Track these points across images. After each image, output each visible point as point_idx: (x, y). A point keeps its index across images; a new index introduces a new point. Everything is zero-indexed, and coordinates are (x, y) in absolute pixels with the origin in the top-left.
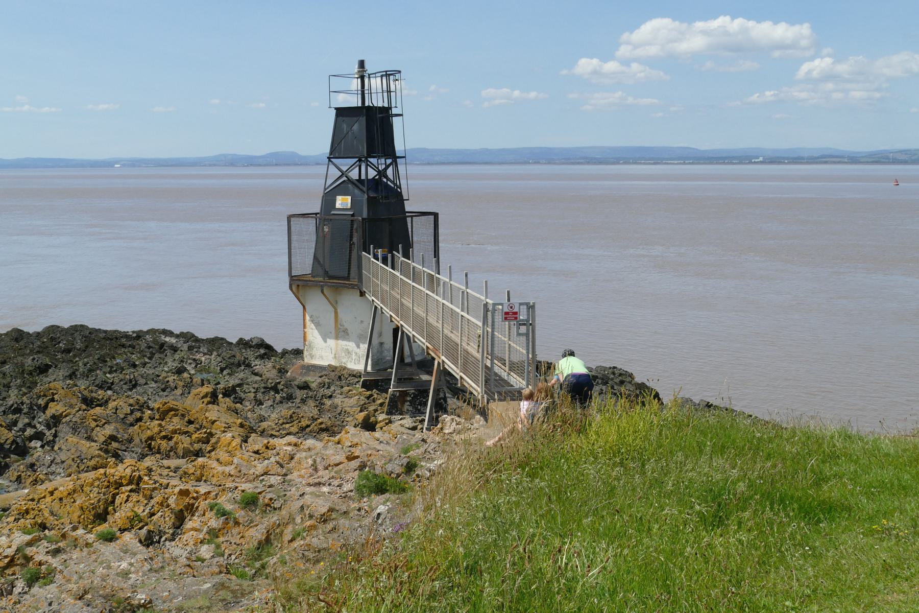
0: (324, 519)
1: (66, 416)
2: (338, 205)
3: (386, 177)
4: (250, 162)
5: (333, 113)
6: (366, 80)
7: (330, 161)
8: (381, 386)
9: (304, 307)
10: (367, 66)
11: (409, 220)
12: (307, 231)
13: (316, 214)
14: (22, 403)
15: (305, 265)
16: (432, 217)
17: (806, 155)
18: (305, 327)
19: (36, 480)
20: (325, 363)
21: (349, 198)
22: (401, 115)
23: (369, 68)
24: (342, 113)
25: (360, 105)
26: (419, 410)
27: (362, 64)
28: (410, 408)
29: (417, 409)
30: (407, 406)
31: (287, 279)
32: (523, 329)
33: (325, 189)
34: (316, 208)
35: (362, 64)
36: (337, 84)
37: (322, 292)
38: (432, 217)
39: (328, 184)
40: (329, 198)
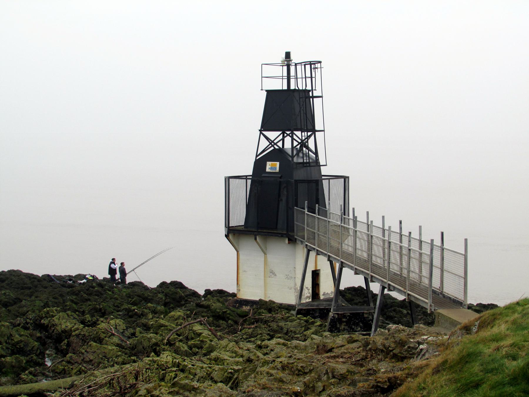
1: (75, 331)
2: (268, 170)
3: (307, 148)
5: (263, 95)
6: (292, 68)
7: (261, 133)
8: (312, 314)
9: (237, 252)
10: (292, 57)
11: (325, 183)
12: (241, 193)
13: (246, 177)
14: (27, 323)
15: (239, 218)
16: (230, 180)
19: (79, 371)
21: (278, 164)
22: (321, 97)
23: (295, 59)
24: (270, 94)
25: (285, 88)
26: (353, 329)
28: (346, 328)
29: (351, 328)
31: (223, 231)
33: (257, 156)
34: (249, 171)
36: (269, 71)
37: (256, 239)
38: (230, 180)
39: (258, 154)
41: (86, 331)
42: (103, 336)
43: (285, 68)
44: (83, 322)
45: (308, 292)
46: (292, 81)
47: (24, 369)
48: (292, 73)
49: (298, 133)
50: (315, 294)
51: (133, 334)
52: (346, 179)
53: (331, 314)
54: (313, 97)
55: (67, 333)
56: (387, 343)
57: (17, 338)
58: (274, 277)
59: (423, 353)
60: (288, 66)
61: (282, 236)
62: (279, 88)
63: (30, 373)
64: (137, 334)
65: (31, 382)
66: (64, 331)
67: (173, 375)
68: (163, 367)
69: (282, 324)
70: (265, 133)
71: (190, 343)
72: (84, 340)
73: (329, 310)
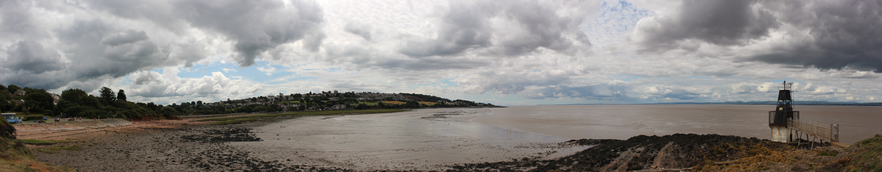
4: (732, 103)
12: (773, 115)
15: (772, 122)
40: (778, 108)
55: (732, 149)
58: (780, 135)
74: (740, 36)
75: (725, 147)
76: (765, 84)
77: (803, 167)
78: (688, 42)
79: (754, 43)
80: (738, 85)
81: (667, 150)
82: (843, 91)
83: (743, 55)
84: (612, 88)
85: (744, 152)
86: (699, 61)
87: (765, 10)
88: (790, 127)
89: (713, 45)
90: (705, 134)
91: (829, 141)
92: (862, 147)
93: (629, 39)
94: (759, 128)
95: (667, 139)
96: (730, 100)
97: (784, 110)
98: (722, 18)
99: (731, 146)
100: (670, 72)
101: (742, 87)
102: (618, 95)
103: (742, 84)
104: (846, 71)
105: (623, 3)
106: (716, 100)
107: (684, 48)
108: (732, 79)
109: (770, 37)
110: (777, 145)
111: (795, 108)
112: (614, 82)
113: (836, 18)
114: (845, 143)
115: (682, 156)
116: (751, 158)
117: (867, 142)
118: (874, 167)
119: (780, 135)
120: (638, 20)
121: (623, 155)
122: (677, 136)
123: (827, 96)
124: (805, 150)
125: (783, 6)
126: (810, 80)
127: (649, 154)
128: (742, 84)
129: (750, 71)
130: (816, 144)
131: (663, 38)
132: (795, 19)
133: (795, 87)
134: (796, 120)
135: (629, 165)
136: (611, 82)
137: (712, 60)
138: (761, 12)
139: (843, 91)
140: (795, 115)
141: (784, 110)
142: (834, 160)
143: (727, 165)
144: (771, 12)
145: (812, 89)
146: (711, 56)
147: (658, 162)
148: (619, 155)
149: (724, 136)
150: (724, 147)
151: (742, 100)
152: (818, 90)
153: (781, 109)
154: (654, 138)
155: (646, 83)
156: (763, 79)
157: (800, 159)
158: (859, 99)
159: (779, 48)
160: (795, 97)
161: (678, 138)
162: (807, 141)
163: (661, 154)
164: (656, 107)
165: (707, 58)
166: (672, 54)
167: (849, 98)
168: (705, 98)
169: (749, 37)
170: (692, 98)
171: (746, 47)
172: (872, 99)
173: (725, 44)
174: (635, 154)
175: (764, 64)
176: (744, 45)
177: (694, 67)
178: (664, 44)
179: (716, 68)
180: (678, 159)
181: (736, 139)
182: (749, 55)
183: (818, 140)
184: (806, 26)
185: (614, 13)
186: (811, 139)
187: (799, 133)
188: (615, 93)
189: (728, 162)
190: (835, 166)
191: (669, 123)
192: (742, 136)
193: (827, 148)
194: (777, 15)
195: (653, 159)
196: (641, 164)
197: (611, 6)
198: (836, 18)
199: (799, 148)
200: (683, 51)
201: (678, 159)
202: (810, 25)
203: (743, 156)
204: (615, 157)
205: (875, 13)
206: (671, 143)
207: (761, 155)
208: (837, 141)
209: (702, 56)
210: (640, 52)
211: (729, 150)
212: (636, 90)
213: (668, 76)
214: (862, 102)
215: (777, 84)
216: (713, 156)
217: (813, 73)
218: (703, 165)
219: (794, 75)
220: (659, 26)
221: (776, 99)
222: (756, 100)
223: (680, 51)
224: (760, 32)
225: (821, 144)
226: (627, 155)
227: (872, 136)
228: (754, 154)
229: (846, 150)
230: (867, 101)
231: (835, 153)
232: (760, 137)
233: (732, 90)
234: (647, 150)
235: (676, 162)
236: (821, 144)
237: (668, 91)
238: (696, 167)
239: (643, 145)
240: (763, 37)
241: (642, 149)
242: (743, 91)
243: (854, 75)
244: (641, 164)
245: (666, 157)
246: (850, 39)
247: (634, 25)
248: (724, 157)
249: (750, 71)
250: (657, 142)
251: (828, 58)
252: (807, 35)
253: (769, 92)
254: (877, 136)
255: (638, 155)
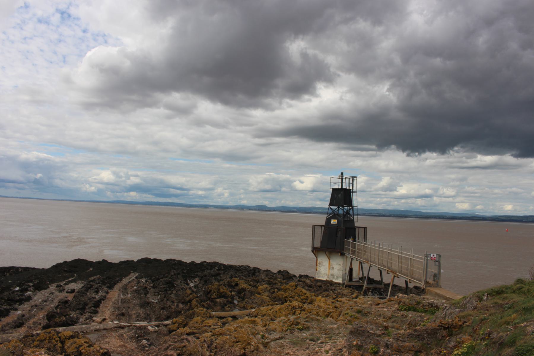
0: (390, 318)
4: (249, 208)
10: (344, 174)
11: (357, 230)
12: (319, 232)
13: (321, 226)
15: (318, 244)
17: (438, 216)
18: (317, 265)
20: (324, 279)
23: (345, 176)
27: (342, 174)
30: (370, 293)
32: (437, 263)
34: (323, 223)
35: (342, 174)
40: (328, 220)
41: (253, 289)
42: (261, 292)
43: (340, 180)
44: (250, 285)
45: (347, 278)
46: (344, 185)
47: (226, 305)
48: (344, 181)
49: (346, 208)
50: (351, 279)
51: (274, 292)
52: (365, 228)
53: (364, 288)
54: (353, 192)
55: (244, 290)
56: (411, 302)
57: (222, 290)
58: (330, 269)
59: (447, 308)
60: (342, 179)
61: (337, 252)
62: (337, 188)
63: (229, 307)
64: (276, 292)
65: (230, 311)
66: (242, 289)
67: (299, 312)
68: (294, 308)
69: (339, 291)
70: (331, 207)
71: (302, 297)
72: (252, 293)
73: (363, 286)
74: (267, 94)
75: (232, 286)
76: (308, 178)
77: (372, 329)
78: (177, 98)
79: (290, 106)
80: (260, 178)
81: (125, 289)
82: (451, 192)
83: (271, 126)
84: (26, 166)
85: (265, 296)
86: (195, 132)
87: (311, 52)
88: (349, 255)
89: (219, 107)
90: (198, 261)
91: (422, 285)
92: (487, 302)
93: (68, 80)
94: (295, 254)
95: (127, 266)
96: (245, 202)
97: (340, 225)
98: (239, 69)
99: (243, 285)
100: (140, 147)
101: (267, 181)
102: (37, 182)
103: (266, 175)
104: (456, 156)
105: (63, 13)
106: (219, 202)
107: (169, 107)
108: (250, 167)
109: (317, 96)
110: (325, 287)
111: (359, 221)
112: (33, 155)
113: (438, 62)
114: (455, 289)
115: (154, 300)
116: (277, 308)
117: (499, 292)
118: (512, 344)
119: (330, 269)
120: (89, 48)
121: (38, 297)
122: (146, 262)
123: (420, 202)
124: (376, 298)
125: (342, 46)
126: (388, 172)
127: (91, 294)
128: (266, 175)
129: (282, 154)
130: (396, 289)
131: (131, 87)
132: (362, 67)
133: (359, 184)
134: (360, 243)
135: (50, 316)
136: (24, 156)
137: (217, 131)
138: (304, 55)
139: (451, 192)
140: (359, 234)
141: (340, 225)
142: (430, 322)
143: (234, 318)
144: (321, 56)
145: (391, 188)
146: (216, 124)
147: (107, 310)
148: (29, 298)
149: (231, 267)
150: (230, 285)
151: (267, 203)
152: (402, 190)
153: (334, 221)
154: (103, 266)
155: (96, 163)
156: (305, 168)
157: (366, 314)
158: (482, 209)
159: (335, 116)
160: (359, 201)
161: (147, 267)
162: (380, 282)
163: (115, 294)
164: (110, 208)
165: (208, 128)
166: (146, 115)
167: (462, 206)
168: (200, 197)
169: (283, 96)
170: (176, 196)
171: (277, 112)
172: (508, 208)
173: (240, 105)
174: (62, 296)
175: (306, 143)
176: (273, 110)
177: (185, 142)
178: (134, 97)
179: (222, 147)
180: (145, 304)
181: (252, 273)
182: (282, 125)
183: (400, 282)
184: (381, 78)
185: (42, 27)
186: (387, 279)
187: (366, 266)
188: (32, 176)
189: (236, 312)
190: (433, 333)
191: (131, 239)
192: (263, 267)
193: (418, 298)
194: (331, 60)
195: (97, 304)
196: (73, 314)
197: (39, 13)
198: (438, 62)
199: (365, 294)
200: (167, 112)
201: (145, 304)
202: (390, 77)
203: (263, 303)
204: (21, 301)
205: (514, 46)
206: (133, 276)
207: (295, 303)
208: (437, 285)
209: (200, 123)
210: (88, 106)
211: (239, 292)
212: (74, 175)
213: (135, 153)
214: (487, 214)
215: (328, 178)
216: (209, 300)
217: (393, 160)
218: (191, 317)
219: (358, 163)
220: (127, 64)
221: (326, 205)
222: (290, 203)
223: (162, 111)
224: (301, 88)
225: (406, 290)
226: (49, 297)
227: (510, 282)
228: (283, 300)
229: (455, 305)
230: (498, 212)
231: (433, 308)
232: (295, 270)
233: (250, 186)
234: (87, 288)
235: (141, 311)
236: (406, 290)
237: (134, 180)
238: (179, 319)
239: (80, 278)
240: (306, 97)
241: (77, 286)
242: (268, 187)
243: (473, 162)
244: (73, 314)
245: (124, 301)
246: (465, 98)
247: (81, 55)
248: (229, 303)
249: (282, 154)
250: (107, 273)
251: (421, 131)
252: (383, 93)
253: (313, 191)
254: (520, 281)
255: (70, 297)
